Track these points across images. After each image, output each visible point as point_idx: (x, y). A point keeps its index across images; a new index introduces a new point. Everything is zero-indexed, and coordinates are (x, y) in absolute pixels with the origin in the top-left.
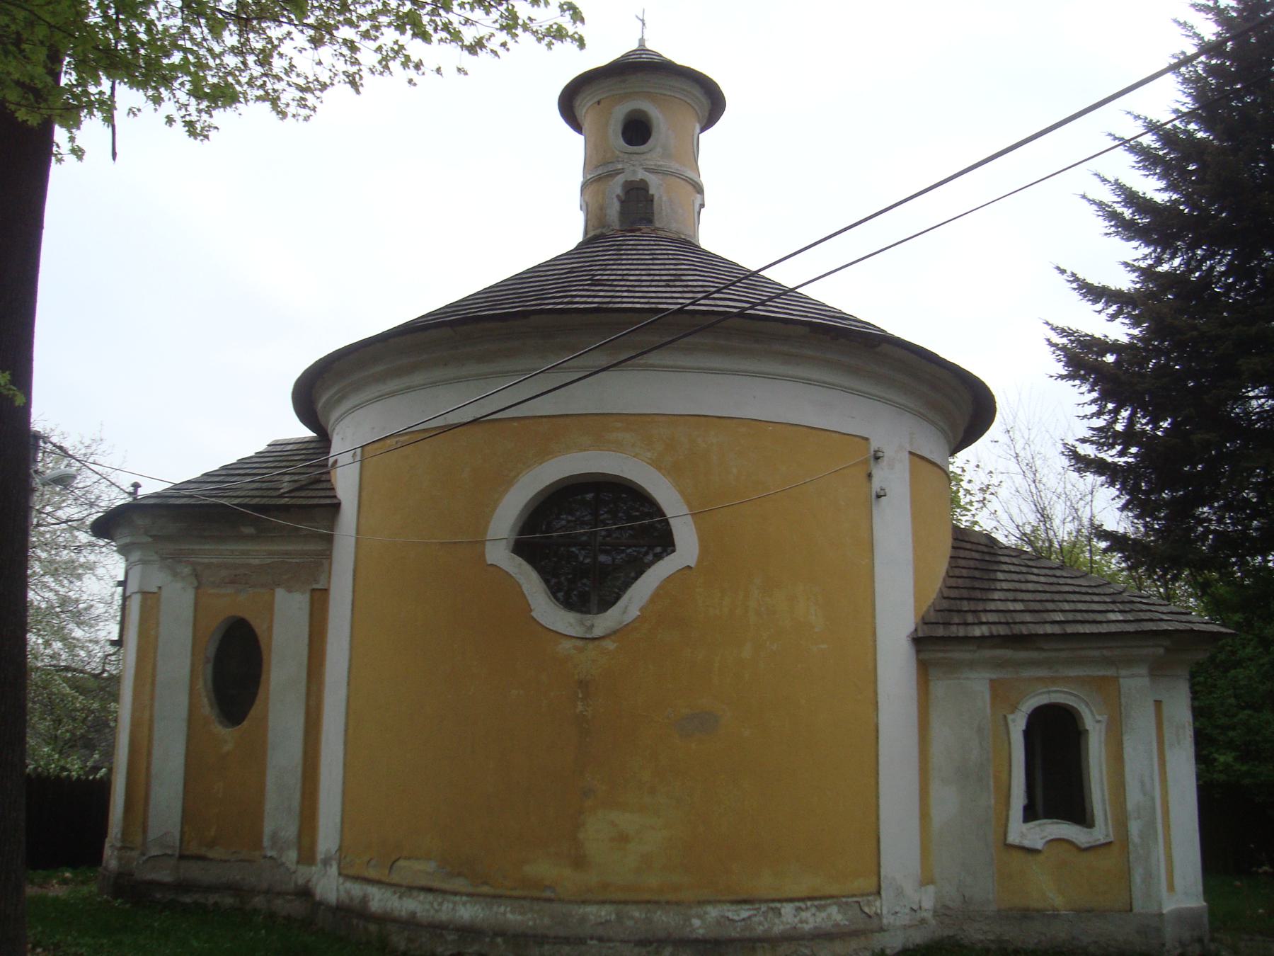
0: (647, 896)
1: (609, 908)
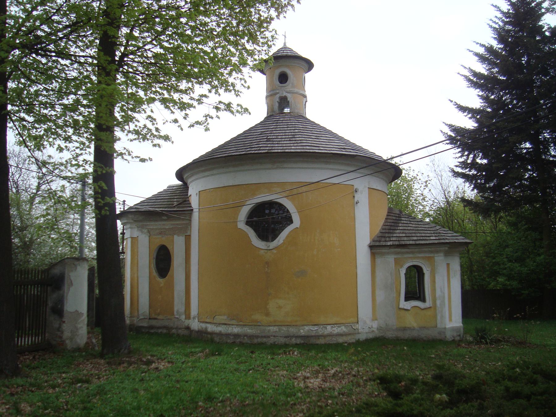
0: (286, 324)
1: (276, 327)
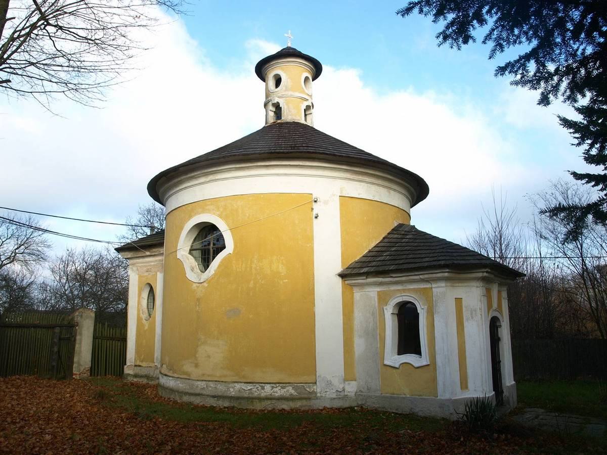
1: (204, 383)
